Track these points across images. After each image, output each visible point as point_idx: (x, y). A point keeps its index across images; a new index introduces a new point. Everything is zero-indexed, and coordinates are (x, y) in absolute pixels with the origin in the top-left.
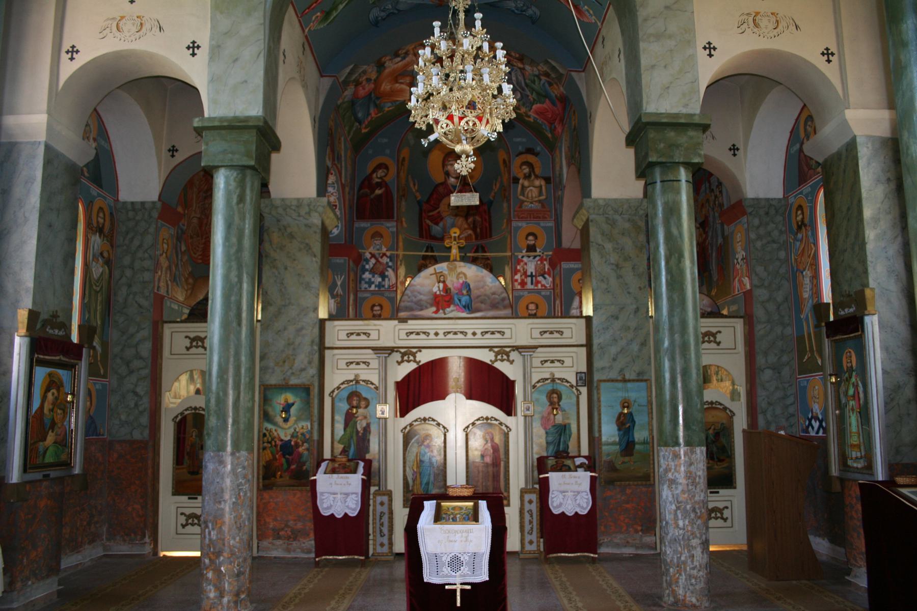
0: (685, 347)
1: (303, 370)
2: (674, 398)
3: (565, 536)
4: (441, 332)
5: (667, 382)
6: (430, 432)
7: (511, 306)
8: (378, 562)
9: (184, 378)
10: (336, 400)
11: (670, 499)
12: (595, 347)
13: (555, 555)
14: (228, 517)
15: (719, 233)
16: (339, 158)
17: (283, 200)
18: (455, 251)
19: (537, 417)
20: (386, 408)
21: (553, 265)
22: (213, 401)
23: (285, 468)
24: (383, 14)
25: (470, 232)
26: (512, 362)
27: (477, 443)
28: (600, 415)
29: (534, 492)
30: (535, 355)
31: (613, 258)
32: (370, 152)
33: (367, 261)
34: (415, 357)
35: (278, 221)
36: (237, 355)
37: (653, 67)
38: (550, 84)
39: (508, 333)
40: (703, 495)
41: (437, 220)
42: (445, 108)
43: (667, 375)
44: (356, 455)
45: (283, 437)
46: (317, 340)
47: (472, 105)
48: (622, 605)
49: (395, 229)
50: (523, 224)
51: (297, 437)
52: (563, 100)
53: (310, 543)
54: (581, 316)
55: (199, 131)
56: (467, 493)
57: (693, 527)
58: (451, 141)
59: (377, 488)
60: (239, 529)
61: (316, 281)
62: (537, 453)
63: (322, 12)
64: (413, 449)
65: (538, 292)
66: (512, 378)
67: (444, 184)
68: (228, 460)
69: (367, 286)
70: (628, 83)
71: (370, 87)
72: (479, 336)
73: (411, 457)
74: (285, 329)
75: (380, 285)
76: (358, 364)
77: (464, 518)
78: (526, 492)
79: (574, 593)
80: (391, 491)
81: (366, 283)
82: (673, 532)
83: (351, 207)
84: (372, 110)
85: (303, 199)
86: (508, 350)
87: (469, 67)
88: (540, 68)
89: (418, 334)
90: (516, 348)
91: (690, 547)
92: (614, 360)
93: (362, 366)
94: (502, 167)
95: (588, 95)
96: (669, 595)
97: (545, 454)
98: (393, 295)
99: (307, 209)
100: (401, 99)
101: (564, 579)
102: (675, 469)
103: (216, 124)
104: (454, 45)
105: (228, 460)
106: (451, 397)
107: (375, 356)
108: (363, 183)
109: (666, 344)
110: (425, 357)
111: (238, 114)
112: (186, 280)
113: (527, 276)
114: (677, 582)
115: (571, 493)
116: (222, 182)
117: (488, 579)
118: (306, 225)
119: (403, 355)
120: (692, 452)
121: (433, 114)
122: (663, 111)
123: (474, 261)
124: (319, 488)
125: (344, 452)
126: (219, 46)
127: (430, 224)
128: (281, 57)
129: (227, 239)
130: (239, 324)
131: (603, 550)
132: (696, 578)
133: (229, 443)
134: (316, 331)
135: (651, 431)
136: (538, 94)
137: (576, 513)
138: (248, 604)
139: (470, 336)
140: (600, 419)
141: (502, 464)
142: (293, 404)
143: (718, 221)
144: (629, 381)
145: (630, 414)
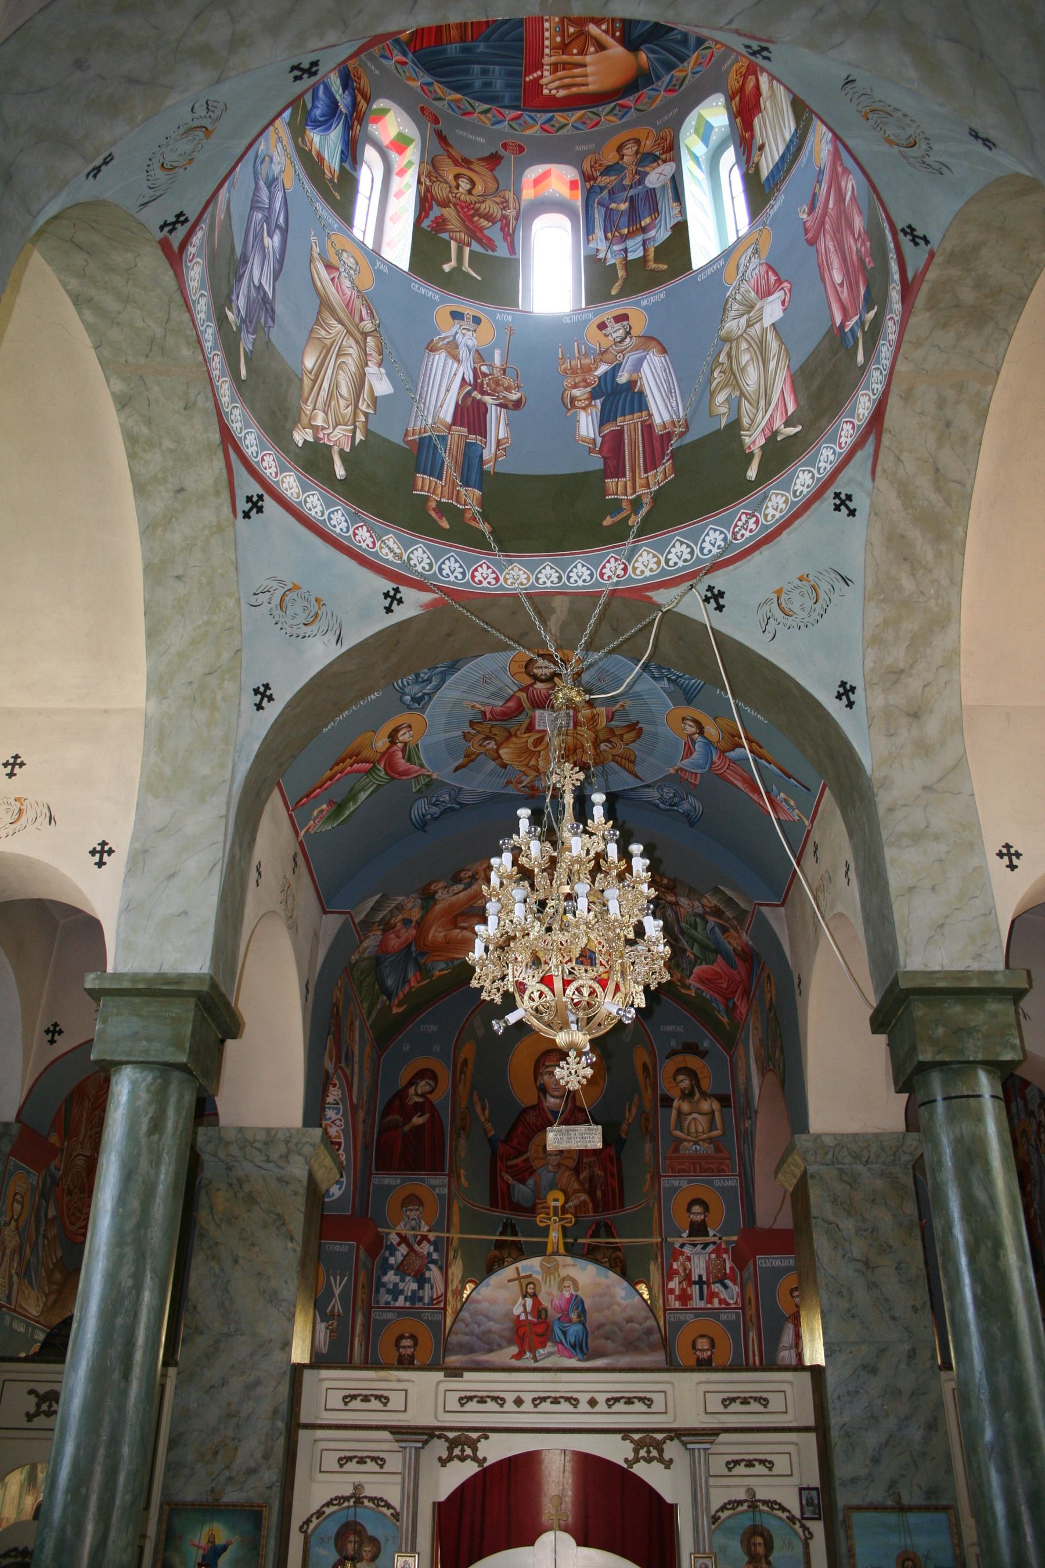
1: (251, 1471)
4: (527, 1398)
5: (1002, 1523)
7: (665, 1346)
12: (834, 1434)
16: (349, 1058)
17: (240, 1130)
18: (555, 1235)
21: (740, 1260)
24: (434, 810)
25: (583, 1197)
26: (668, 1464)
30: (714, 1448)
31: (858, 1248)
33: (392, 1249)
34: (475, 1450)
35: (229, 1168)
36: (115, 1441)
37: (911, 889)
38: (724, 930)
41: (524, 1173)
42: (536, 962)
46: (284, 1408)
47: (587, 957)
49: (446, 1190)
50: (684, 1183)
52: (748, 956)
55: (96, 994)
58: (549, 1026)
61: (289, 1287)
63: (331, 803)
65: (714, 1314)
66: (669, 1499)
67: (538, 1107)
69: (389, 1298)
70: (867, 919)
71: (409, 933)
74: (224, 1383)
75: (414, 1298)
81: (388, 1292)
83: (367, 1147)
85: (278, 1130)
86: (660, 1437)
87: (582, 888)
89: (482, 1400)
90: (677, 1434)
92: (876, 1460)
99: (283, 1149)
103: (126, 985)
104: (555, 850)
106: (547, 1539)
107: (395, 1446)
108: (390, 1103)
109: (988, 1434)
110: (496, 1450)
111: (166, 969)
113: (691, 1283)
116: (125, 1091)
118: (280, 1179)
119: (452, 1444)
121: (519, 972)
122: (937, 968)
123: (590, 1254)
126: (145, 851)
127: (511, 1181)
129: (121, 1200)
130: (126, 1377)
134: (284, 1389)
136: (703, 947)
139: (584, 1406)
142: (224, 1548)
144: (911, 1509)
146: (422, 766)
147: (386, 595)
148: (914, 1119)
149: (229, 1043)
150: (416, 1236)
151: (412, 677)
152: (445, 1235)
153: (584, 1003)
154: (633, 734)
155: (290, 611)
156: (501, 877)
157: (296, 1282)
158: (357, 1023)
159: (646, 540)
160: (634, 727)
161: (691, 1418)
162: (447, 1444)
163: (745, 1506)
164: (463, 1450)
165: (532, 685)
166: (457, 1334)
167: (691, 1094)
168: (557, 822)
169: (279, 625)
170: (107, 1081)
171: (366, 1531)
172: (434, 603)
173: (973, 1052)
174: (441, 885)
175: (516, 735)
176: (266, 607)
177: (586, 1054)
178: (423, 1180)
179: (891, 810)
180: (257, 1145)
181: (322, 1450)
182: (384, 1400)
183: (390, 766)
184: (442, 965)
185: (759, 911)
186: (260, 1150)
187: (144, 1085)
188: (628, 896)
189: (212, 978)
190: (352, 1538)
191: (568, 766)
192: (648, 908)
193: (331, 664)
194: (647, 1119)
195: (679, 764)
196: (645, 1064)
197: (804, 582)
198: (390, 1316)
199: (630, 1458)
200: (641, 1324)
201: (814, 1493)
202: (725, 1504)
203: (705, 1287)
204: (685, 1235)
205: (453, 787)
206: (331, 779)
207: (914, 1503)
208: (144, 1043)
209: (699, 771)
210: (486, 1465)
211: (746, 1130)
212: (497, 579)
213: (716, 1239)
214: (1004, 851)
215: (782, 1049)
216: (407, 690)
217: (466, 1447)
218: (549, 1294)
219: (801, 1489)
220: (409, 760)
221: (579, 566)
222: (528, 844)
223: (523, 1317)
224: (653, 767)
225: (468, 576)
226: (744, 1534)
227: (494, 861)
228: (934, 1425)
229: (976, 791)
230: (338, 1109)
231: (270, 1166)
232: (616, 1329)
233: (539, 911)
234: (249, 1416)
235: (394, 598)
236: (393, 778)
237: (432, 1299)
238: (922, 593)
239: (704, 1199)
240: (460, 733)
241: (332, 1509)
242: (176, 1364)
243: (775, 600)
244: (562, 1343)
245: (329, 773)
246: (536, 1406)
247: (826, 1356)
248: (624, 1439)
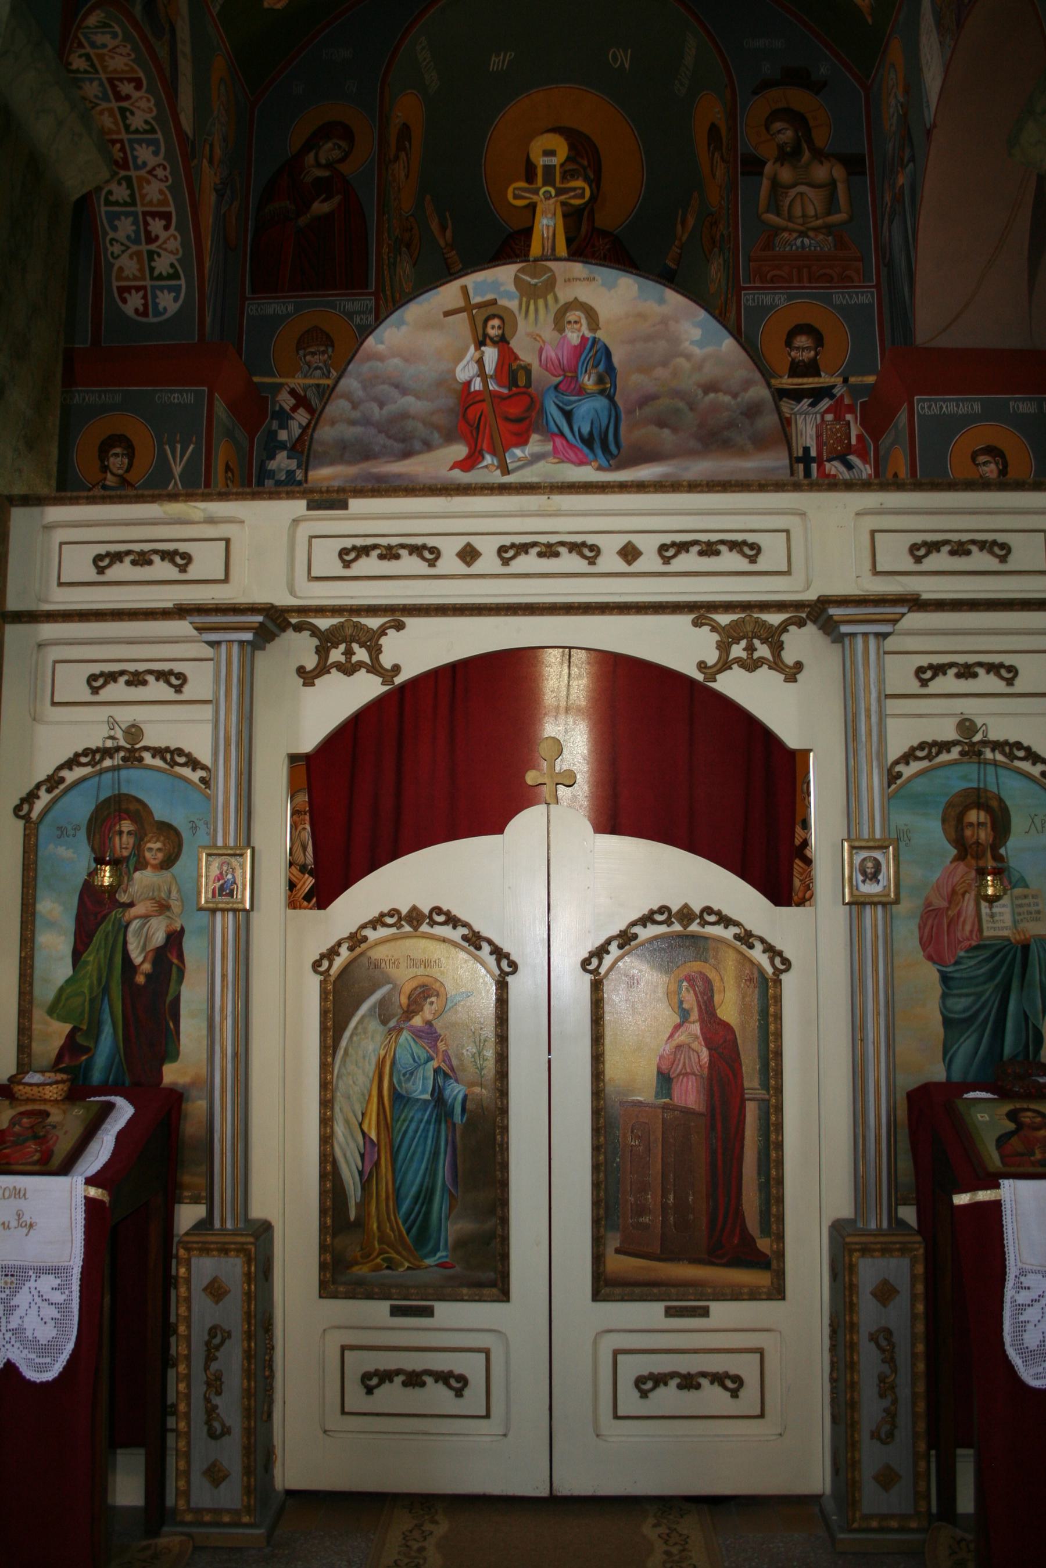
4: (487, 547)
18: (548, 224)
26: (792, 673)
27: (645, 1006)
33: (283, 418)
34: (375, 651)
50: (780, 299)
59: (199, 1211)
66: (792, 741)
72: (650, 561)
78: (866, 1250)
80: (265, 1229)
86: (775, 619)
89: (390, 554)
90: (818, 613)
97: (938, 1073)
110: (419, 650)
119: (326, 641)
141: (751, 1111)
161: (841, 574)
162: (315, 642)
164: (349, 653)
166: (333, 423)
171: (150, 813)
181: (55, 662)
182: (181, 559)
199: (711, 662)
200: (735, 396)
202: (913, 749)
203: (814, 466)
210: (399, 680)
217: (355, 646)
218: (535, 337)
223: (477, 385)
226: (950, 805)
230: (154, 143)
232: (681, 405)
239: (817, 325)
241: (79, 772)
244: (562, 435)
246: (506, 562)
248: (696, 624)
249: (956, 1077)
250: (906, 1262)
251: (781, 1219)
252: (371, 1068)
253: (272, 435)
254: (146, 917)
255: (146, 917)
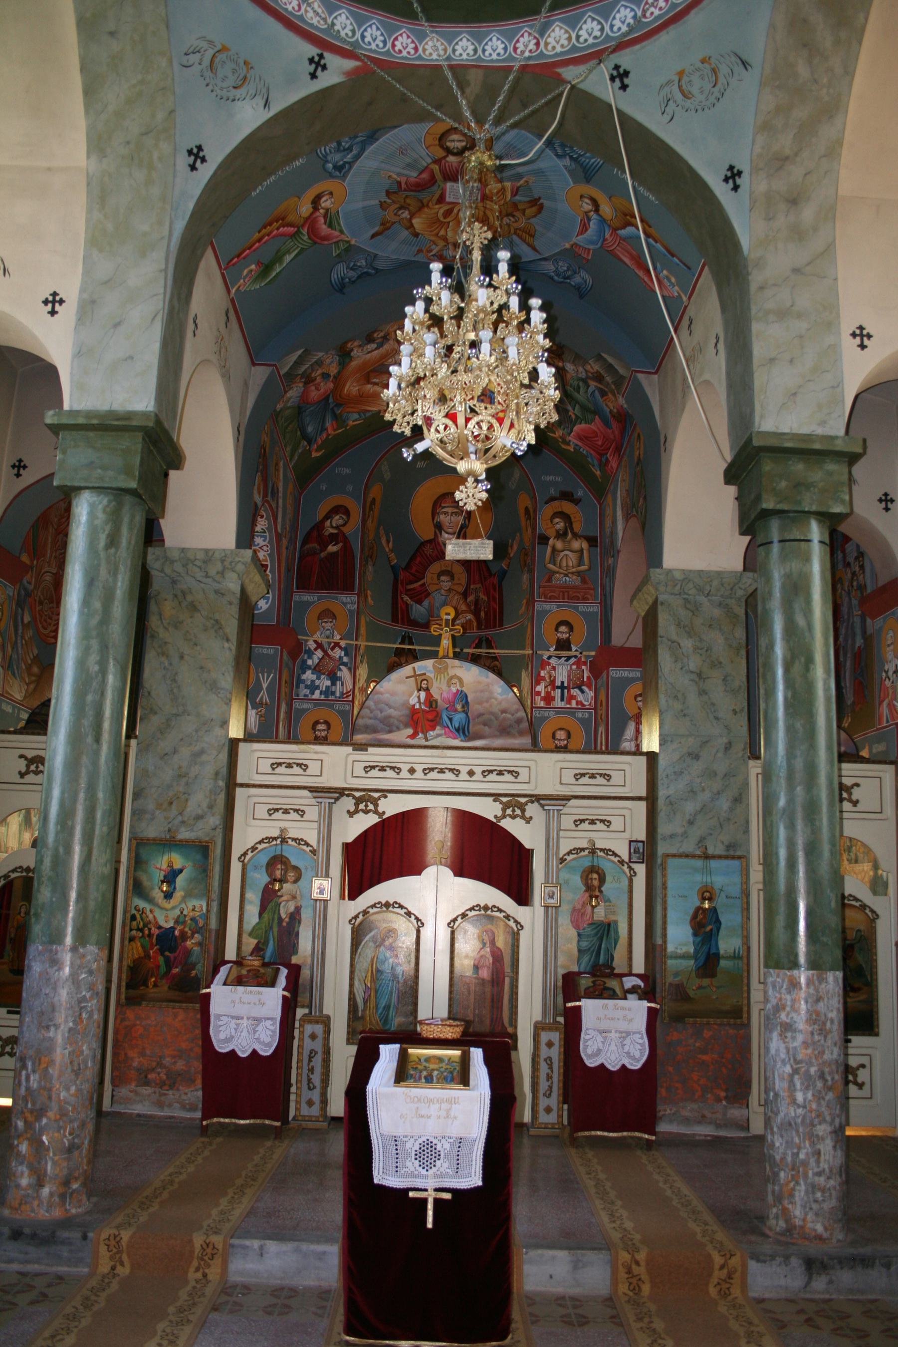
0: (811, 809)
1: (199, 817)
2: (791, 891)
3: (606, 1102)
4: (419, 768)
5: (782, 863)
6: (396, 926)
7: (532, 734)
8: (302, 1132)
9: (15, 821)
10: (249, 867)
11: (783, 1055)
12: (661, 802)
13: (587, 1133)
14: (60, 1054)
15: (858, 631)
16: (275, 493)
17: (183, 550)
18: (446, 642)
19: (566, 909)
20: (326, 884)
21: (597, 670)
22: (47, 862)
23: (162, 973)
24: (352, 274)
25: (470, 616)
26: (528, 820)
27: (469, 945)
28: (665, 909)
29: (557, 1029)
32: (323, 487)
33: (310, 653)
35: (174, 582)
36: (91, 789)
37: (772, 360)
38: (603, 393)
39: (524, 775)
40: (836, 1050)
41: (420, 596)
42: (442, 399)
43: (782, 853)
44: (276, 957)
45: (162, 923)
46: (224, 771)
47: (487, 396)
48: (698, 1230)
50: (552, 607)
51: (184, 923)
52: (622, 418)
53: (195, 1094)
54: (638, 752)
55: (56, 429)
56: (451, 1032)
57: (819, 1105)
59: (306, 1011)
60: (77, 1073)
61: (227, 680)
62: (563, 967)
63: (259, 264)
64: (367, 951)
65: (571, 712)
66: (527, 845)
68: (67, 958)
69: (307, 692)
70: (730, 386)
72: (478, 776)
73: (363, 964)
74: (175, 751)
75: (328, 692)
76: (286, 812)
77: (445, 1079)
78: (543, 1029)
79: (619, 1203)
80: (328, 1017)
81: (307, 687)
82: (786, 1111)
83: (289, 570)
84: (328, 424)
85: (214, 551)
86: (523, 800)
87: (486, 334)
88: (588, 367)
89: (383, 769)
90: (537, 798)
91: (814, 1139)
92: (691, 823)
93: (293, 816)
94: (523, 518)
95: (661, 411)
96: (777, 1217)
98: (348, 707)
99: (219, 566)
100: (374, 409)
101: (602, 1176)
102: (792, 1006)
103: (81, 421)
104: (463, 301)
105: (67, 958)
106: (430, 872)
109: (782, 802)
110: (392, 806)
112: (29, 668)
113: (554, 687)
114: (791, 1195)
115: (616, 1034)
116: (85, 512)
117: (480, 1183)
118: (217, 592)
119: (358, 801)
120: (821, 980)
121: (426, 408)
122: (787, 430)
123: (475, 660)
124: (216, 1007)
125: (258, 950)
127: (409, 601)
128: (191, 326)
129: (86, 602)
130: (98, 740)
131: (663, 1127)
132: (823, 1191)
133: (70, 929)
134: (224, 756)
135: (746, 939)
136: (584, 408)
137: (624, 1066)
138: (84, 1198)
139: (464, 776)
140: (665, 916)
141: (507, 980)
142: (181, 871)
143: (857, 612)
144: (714, 857)
145: (714, 910)
146: (341, 232)
147: (311, 61)
148: (751, 562)
149: (173, 474)
150: (330, 643)
151: (334, 145)
152: (354, 643)
153: (482, 436)
154: (534, 209)
155: (221, 73)
156: (414, 323)
157: (232, 674)
158: (281, 464)
159: (559, 15)
160: (535, 202)
163: (586, 852)
164: (366, 806)
165: (445, 157)
167: (565, 534)
168: (465, 278)
169: (210, 87)
170: (68, 510)
172: (356, 71)
173: (809, 503)
174: (356, 343)
175: (427, 206)
176: (197, 68)
177: (481, 481)
178: (336, 598)
179: (762, 288)
180: (198, 563)
182: (304, 767)
183: (313, 231)
184: (356, 416)
185: (636, 378)
186: (200, 567)
187: (100, 507)
188: (526, 348)
189: (156, 415)
190: (279, 866)
191: (477, 225)
192: (543, 356)
193: (260, 128)
194: (526, 554)
195: (574, 240)
196: (527, 508)
197: (706, 65)
198: (308, 706)
201: (641, 845)
204: (552, 649)
205: (369, 253)
206: (259, 240)
207: (717, 853)
208: (99, 471)
209: (591, 247)
211: (609, 566)
212: (416, 49)
213: (577, 654)
214: (858, 332)
215: (645, 498)
216: (329, 158)
218: (440, 689)
219: (631, 842)
220: (330, 226)
221: (494, 39)
222: (439, 295)
223: (417, 706)
224: (550, 242)
225: (389, 45)
226: (584, 871)
227: (408, 309)
228: (740, 799)
229: (839, 277)
231: (209, 580)
233: (446, 356)
234: (196, 777)
235: (318, 64)
236: (315, 243)
237: (342, 694)
238: (816, 81)
240: (377, 202)
242: (136, 737)
243: (676, 82)
245: (257, 236)
247: (660, 745)
249: (582, 970)
250: (557, 1034)
251: (516, 1020)
252: (369, 960)
253: (305, 662)
254: (287, 901)
255: (287, 901)
